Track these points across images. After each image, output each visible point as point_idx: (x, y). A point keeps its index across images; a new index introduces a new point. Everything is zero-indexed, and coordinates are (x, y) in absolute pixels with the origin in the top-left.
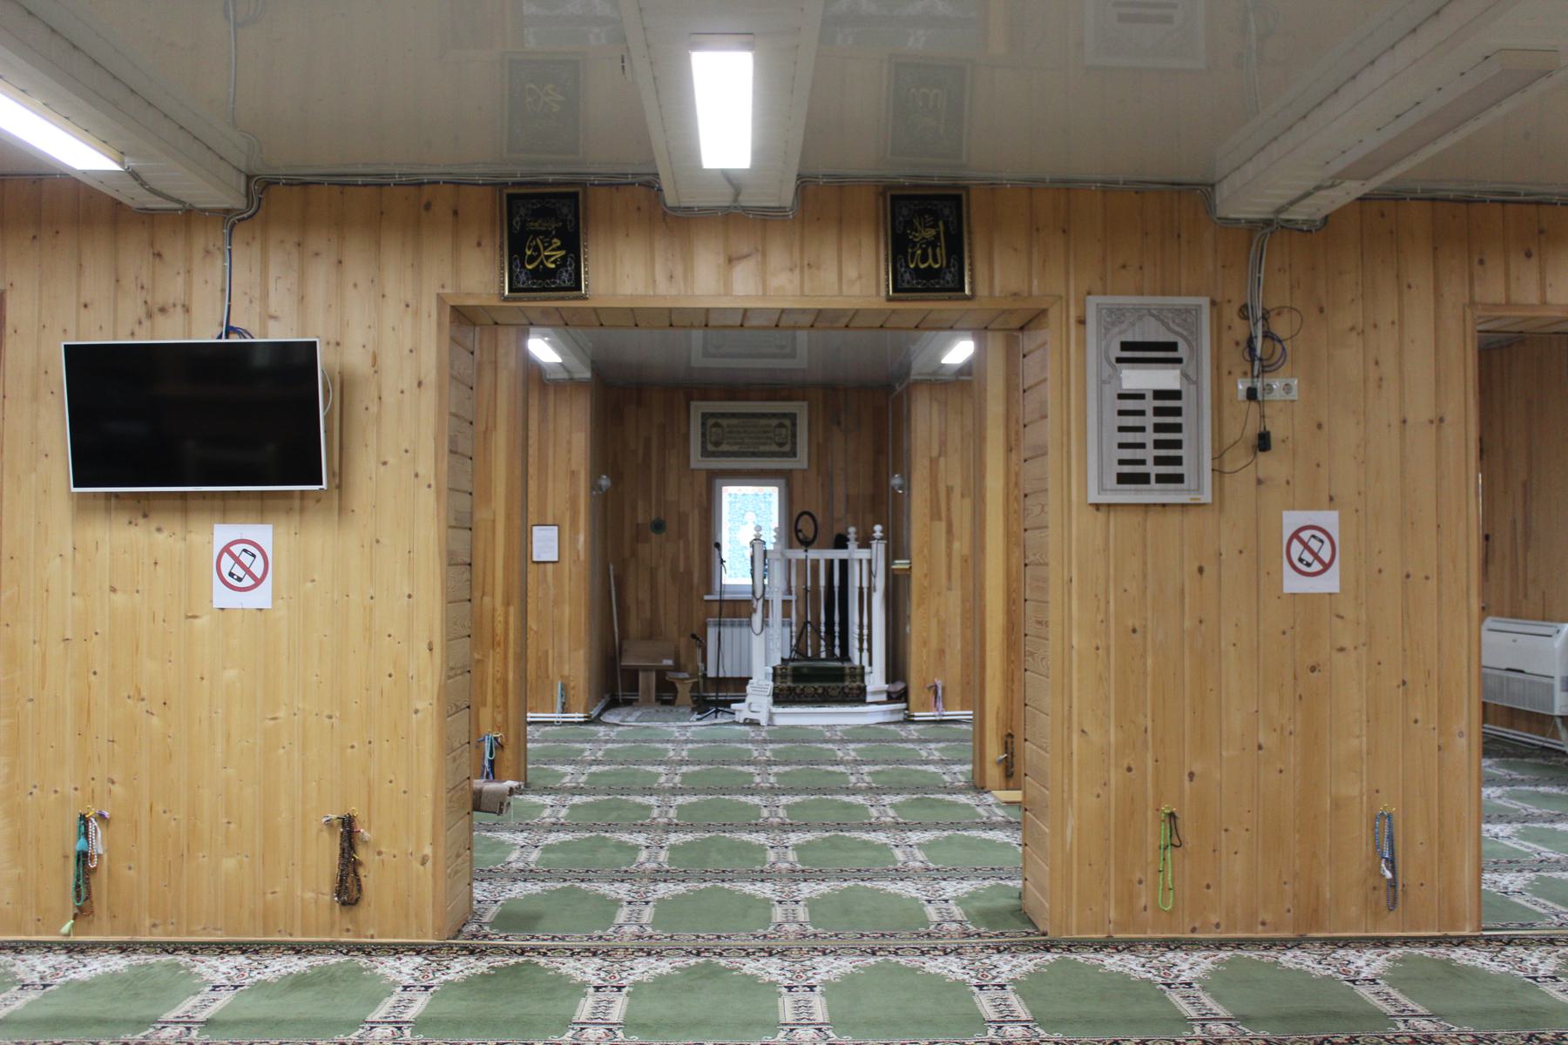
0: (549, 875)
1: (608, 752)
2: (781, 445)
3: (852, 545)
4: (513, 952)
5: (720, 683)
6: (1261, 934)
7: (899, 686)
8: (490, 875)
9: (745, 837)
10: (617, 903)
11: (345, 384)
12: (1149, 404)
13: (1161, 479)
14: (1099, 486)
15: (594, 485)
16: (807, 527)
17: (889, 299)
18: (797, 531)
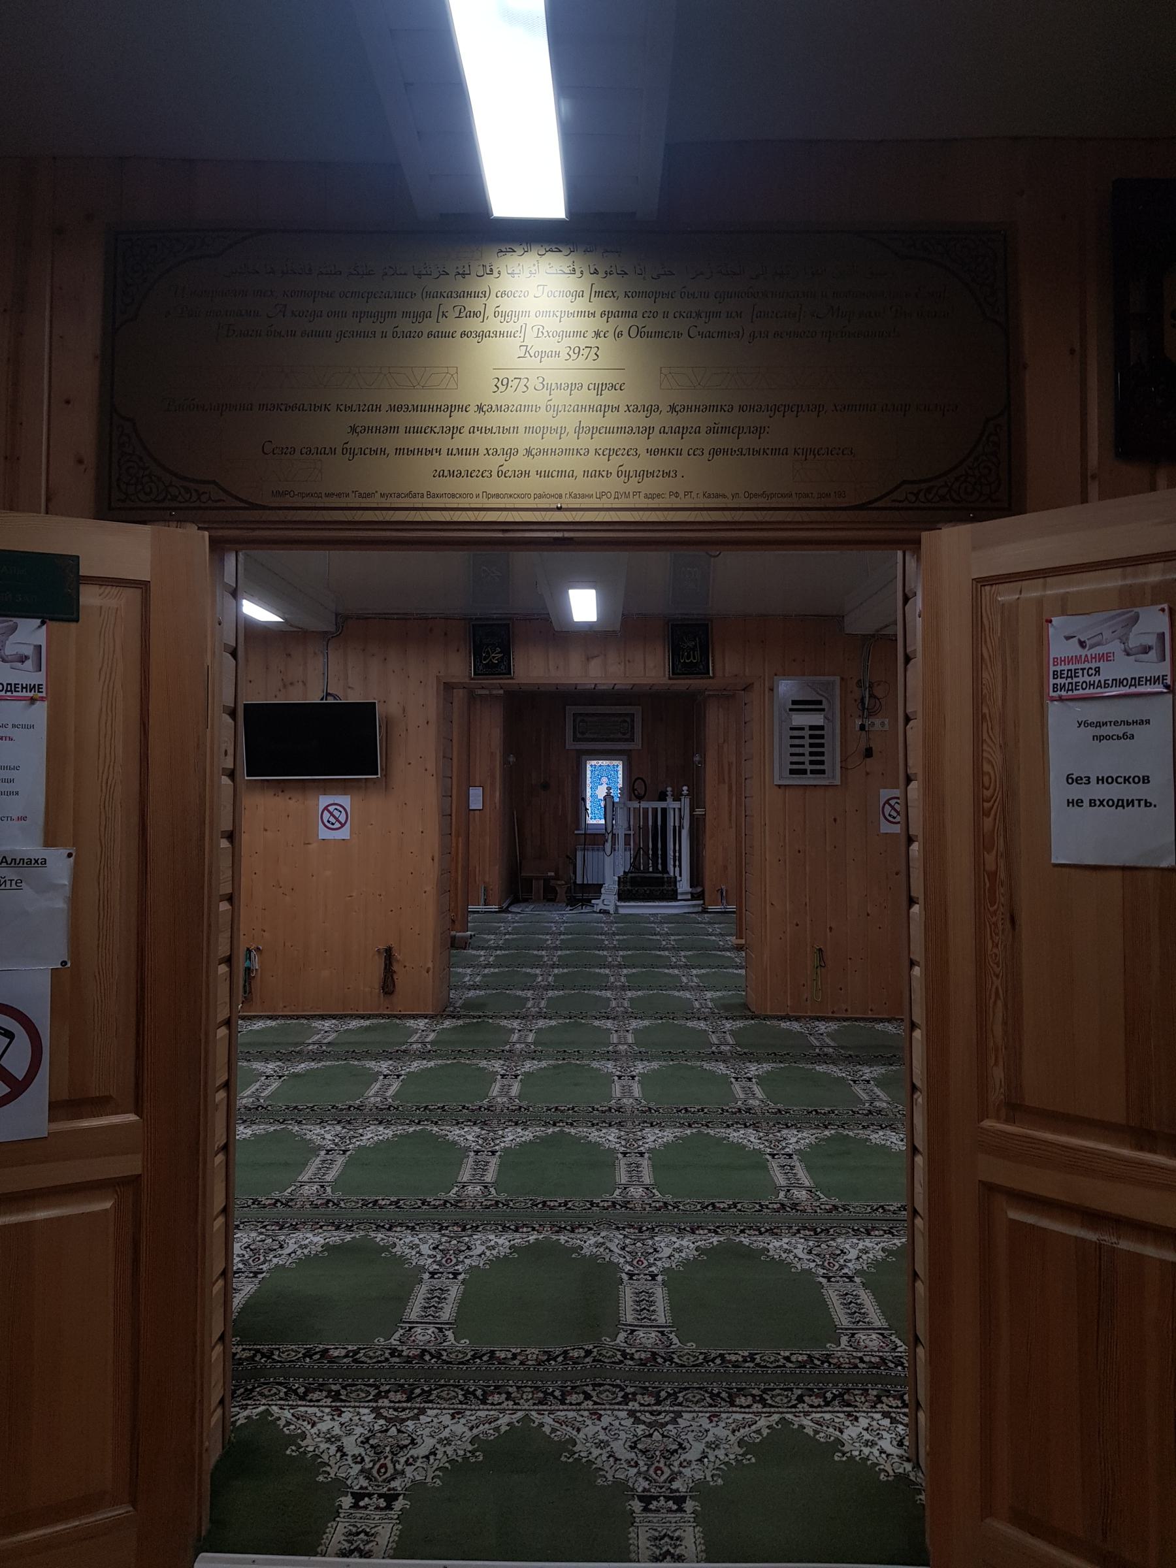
0: (487, 987)
1: (514, 928)
2: (624, 734)
3: (669, 799)
4: (474, 1017)
5: (585, 887)
6: (870, 1015)
7: (699, 889)
8: (456, 988)
9: (597, 970)
10: (527, 999)
11: (388, 722)
12: (806, 733)
13: (812, 772)
14: (779, 775)
15: (505, 762)
16: (640, 789)
17: (670, 679)
18: (634, 790)
